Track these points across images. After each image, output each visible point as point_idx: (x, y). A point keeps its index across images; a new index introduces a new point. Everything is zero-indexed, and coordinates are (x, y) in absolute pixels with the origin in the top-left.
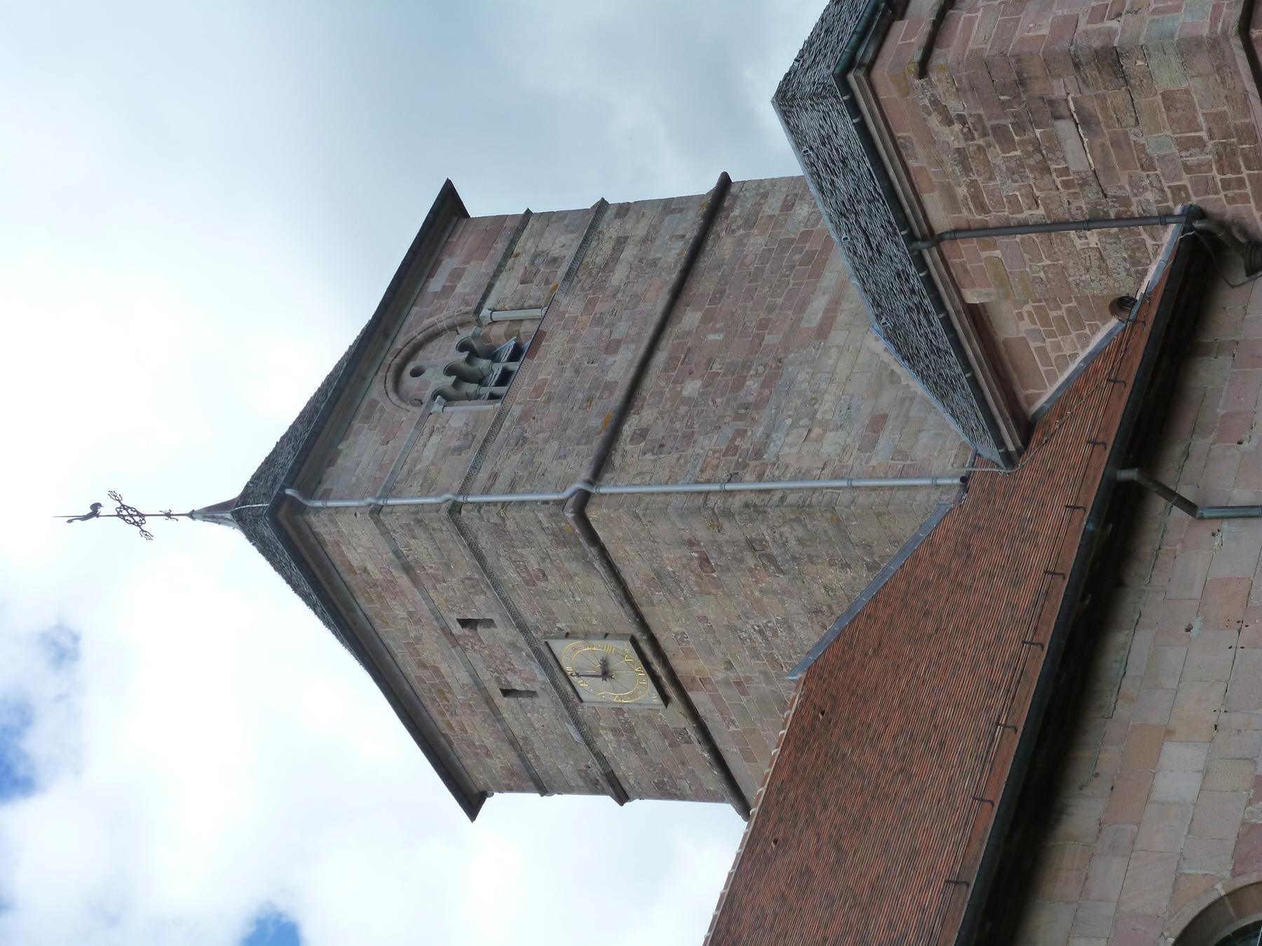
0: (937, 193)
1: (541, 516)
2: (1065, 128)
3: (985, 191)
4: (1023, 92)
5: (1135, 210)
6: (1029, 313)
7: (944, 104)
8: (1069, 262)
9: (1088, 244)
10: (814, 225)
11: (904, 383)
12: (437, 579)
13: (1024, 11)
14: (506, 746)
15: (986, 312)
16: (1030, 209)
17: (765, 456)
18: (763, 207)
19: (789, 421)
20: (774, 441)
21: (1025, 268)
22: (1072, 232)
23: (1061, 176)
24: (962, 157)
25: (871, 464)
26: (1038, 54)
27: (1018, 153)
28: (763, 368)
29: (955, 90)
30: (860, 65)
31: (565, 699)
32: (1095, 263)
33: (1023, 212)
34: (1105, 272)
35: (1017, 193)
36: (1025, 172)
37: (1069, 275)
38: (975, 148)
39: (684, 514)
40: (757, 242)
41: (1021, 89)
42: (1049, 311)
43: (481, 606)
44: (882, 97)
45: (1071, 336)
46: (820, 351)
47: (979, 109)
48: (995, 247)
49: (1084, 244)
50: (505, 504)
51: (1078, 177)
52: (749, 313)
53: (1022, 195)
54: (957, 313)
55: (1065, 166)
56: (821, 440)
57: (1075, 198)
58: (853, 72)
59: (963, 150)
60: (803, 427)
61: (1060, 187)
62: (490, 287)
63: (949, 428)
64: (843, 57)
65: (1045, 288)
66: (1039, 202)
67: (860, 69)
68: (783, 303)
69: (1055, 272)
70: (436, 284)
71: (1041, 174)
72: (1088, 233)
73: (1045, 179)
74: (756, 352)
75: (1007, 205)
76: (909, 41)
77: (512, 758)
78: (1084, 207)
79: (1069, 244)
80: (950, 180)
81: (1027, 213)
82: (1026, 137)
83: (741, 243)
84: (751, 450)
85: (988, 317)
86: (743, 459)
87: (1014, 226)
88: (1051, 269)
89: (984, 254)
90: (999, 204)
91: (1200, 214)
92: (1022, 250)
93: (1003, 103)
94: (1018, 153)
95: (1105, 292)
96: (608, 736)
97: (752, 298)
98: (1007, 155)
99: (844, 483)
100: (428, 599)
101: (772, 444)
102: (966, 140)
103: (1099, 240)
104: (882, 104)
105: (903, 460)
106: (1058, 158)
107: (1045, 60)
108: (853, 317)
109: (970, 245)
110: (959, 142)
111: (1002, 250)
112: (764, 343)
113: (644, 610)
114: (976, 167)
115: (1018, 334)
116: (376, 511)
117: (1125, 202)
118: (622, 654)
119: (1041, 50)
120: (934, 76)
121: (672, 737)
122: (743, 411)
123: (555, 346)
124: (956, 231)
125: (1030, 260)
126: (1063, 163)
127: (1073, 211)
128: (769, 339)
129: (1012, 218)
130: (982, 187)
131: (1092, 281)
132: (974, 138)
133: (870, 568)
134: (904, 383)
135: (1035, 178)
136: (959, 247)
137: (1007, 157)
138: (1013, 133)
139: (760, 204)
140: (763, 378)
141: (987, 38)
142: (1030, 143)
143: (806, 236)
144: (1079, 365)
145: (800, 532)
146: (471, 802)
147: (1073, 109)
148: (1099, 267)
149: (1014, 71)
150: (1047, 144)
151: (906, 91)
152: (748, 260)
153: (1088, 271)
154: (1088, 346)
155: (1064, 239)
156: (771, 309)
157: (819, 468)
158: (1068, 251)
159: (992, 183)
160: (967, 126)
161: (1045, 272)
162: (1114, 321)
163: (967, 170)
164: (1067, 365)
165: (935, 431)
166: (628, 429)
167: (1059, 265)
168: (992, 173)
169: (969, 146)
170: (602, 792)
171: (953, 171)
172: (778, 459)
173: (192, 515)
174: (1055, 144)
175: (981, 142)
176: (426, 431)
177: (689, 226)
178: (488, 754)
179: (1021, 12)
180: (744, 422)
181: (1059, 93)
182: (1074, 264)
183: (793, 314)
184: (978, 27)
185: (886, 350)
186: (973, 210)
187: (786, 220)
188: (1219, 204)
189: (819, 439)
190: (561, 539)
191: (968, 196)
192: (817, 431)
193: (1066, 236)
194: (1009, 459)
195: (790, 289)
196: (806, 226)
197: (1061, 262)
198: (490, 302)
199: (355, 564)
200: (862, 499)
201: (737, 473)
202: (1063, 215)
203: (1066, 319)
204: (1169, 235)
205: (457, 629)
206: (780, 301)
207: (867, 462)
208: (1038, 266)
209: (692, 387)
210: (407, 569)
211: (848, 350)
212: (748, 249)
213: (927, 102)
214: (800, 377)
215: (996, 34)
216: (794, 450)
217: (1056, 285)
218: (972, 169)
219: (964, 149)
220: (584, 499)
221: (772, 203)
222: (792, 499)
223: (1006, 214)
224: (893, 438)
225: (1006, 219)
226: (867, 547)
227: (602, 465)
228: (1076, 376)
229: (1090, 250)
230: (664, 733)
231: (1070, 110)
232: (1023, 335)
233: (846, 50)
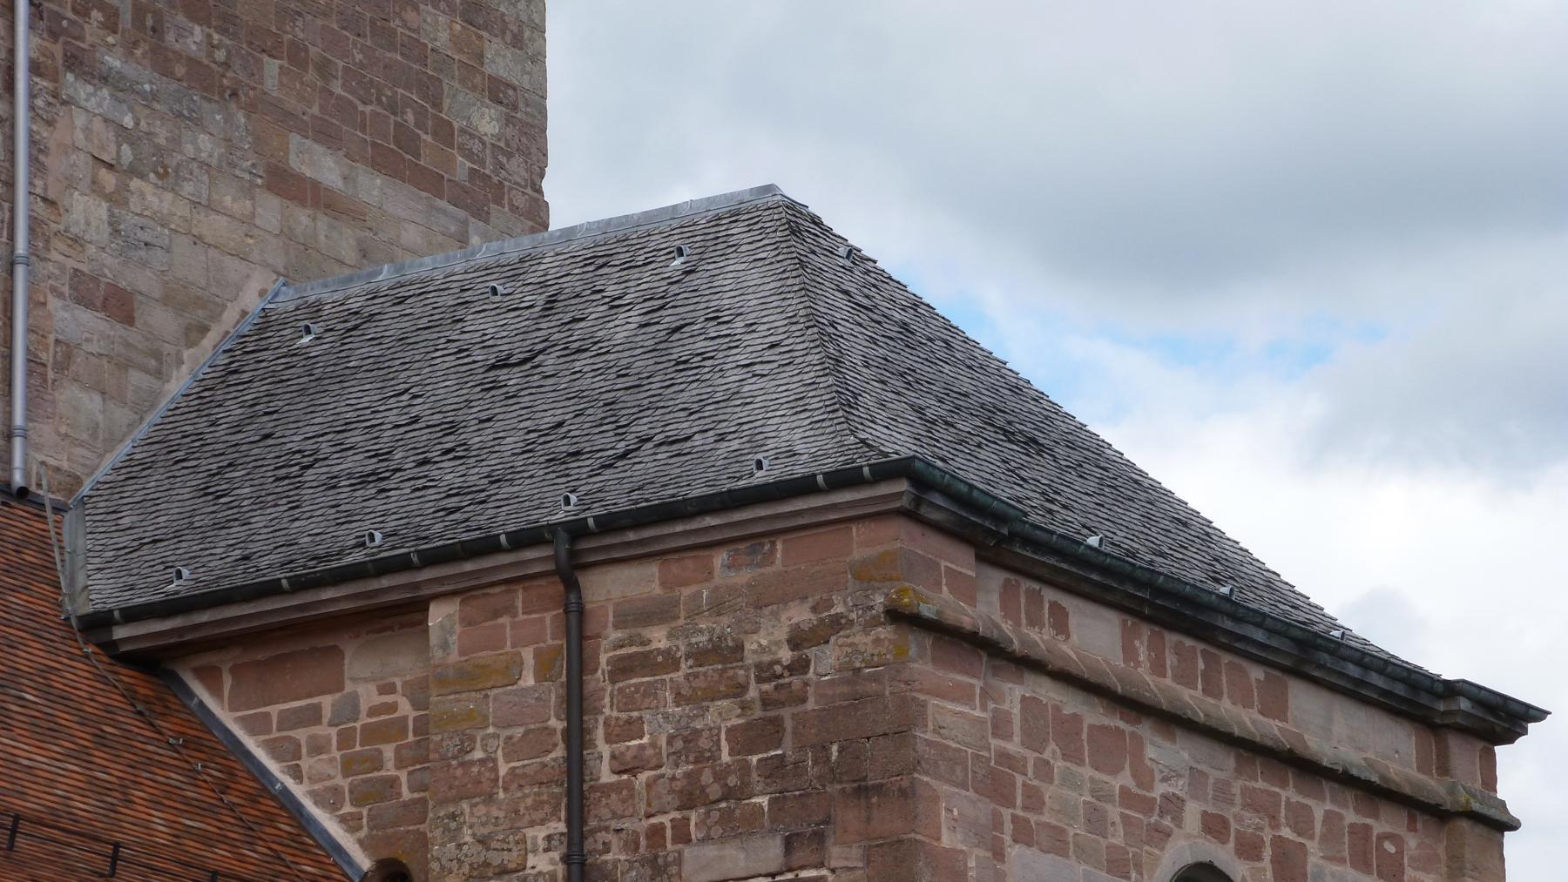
0: (657, 590)
3: (656, 681)
4: (843, 789)
6: (392, 707)
7: (833, 639)
8: (500, 809)
9: (535, 851)
10: (461, 148)
11: (186, 354)
13: (977, 796)
15: (402, 626)
16: (613, 757)
17: (70, 77)
18: (498, 40)
19: (128, 121)
20: (94, 95)
21: (494, 725)
22: (562, 827)
23: (673, 828)
24: (725, 652)
25: (50, 298)
26: (913, 831)
27: (725, 757)
28: (223, 59)
29: (858, 665)
30: (918, 501)
32: (496, 859)
33: (607, 742)
34: (475, 873)
35: (645, 740)
36: (687, 763)
37: (473, 806)
38: (741, 680)
41: (848, 786)
42: (394, 745)
44: (854, 530)
45: (340, 776)
46: (247, 177)
47: (816, 702)
48: (542, 674)
49: (535, 844)
51: (670, 859)
52: (319, 22)
53: (642, 747)
54: (416, 586)
55: (693, 837)
56: (93, 191)
57: (626, 843)
58: (911, 490)
59: (739, 656)
60: (118, 152)
61: (653, 820)
63: (106, 452)
64: (937, 472)
65: (450, 755)
66: (625, 777)
67: (913, 500)
68: (332, 93)
69: (484, 780)
71: (681, 792)
72: (556, 855)
73: (670, 798)
74: (250, 44)
75: (624, 716)
76: (944, 582)
78: (609, 857)
79: (538, 815)
80: (681, 621)
81: (605, 749)
82: (755, 776)
84: (82, 45)
85: (391, 628)
86: (66, 29)
87: (582, 720)
88: (487, 774)
89: (528, 655)
90: (627, 702)
92: (532, 727)
93: (825, 749)
94: (725, 757)
95: (435, 866)
97: (344, 28)
98: (723, 736)
99: (21, 247)
101: (90, 89)
102: (758, 666)
103: (540, 873)
104: (843, 526)
105: (55, 363)
106: (710, 828)
107: (900, 842)
108: (302, 241)
109: (549, 631)
110: (755, 652)
111: (533, 689)
112: (266, 58)
114: (705, 674)
115: (351, 679)
119: (919, 837)
120: (885, 632)
122: (149, 22)
124: (581, 612)
125: (510, 738)
126: (700, 836)
127: (602, 836)
128: (272, 67)
129: (597, 720)
130: (664, 677)
131: (459, 846)
132: (760, 680)
134: (186, 354)
135: (673, 778)
136: (547, 610)
137: (718, 735)
138: (765, 755)
139: (504, 33)
140: (206, 62)
141: (942, 731)
142: (742, 783)
143: (444, 132)
144: (277, 780)
147: (804, 874)
148: (486, 864)
149: (883, 781)
150: (738, 812)
151: (866, 575)
152: (410, 15)
153: (479, 841)
154: (316, 803)
155: (547, 809)
156: (324, 69)
157: (45, 189)
158: (522, 811)
159: (669, 696)
160: (786, 673)
161: (482, 762)
162: (365, 863)
163: (699, 656)
164: (278, 757)
165: (101, 425)
167: (495, 790)
168: (688, 700)
169: (747, 669)
171: (701, 631)
172: (64, 103)
174: (737, 827)
175: (752, 693)
179: (976, 792)
180: (129, 26)
182: (497, 818)
183: (313, 116)
184: (960, 712)
185: (244, 313)
186: (618, 652)
187: (474, 88)
189: (96, 187)
191: (647, 648)
192: (109, 179)
193: (556, 809)
194: (96, 624)
195: (355, 107)
196: (463, 131)
197: (501, 795)
201: (41, 18)
202: (596, 816)
203: (376, 774)
206: (337, 88)
207: (54, 290)
208: (496, 752)
211: (247, 235)
212: (428, 12)
213: (839, 609)
214: (204, 141)
215: (947, 747)
216: (79, 136)
217: (455, 778)
218: (701, 666)
219: (742, 659)
221: (504, 56)
223: (607, 711)
224: (92, 340)
225: (595, 708)
228: (253, 770)
229: (523, 852)
231: (803, 868)
232: (349, 687)
233: (947, 476)
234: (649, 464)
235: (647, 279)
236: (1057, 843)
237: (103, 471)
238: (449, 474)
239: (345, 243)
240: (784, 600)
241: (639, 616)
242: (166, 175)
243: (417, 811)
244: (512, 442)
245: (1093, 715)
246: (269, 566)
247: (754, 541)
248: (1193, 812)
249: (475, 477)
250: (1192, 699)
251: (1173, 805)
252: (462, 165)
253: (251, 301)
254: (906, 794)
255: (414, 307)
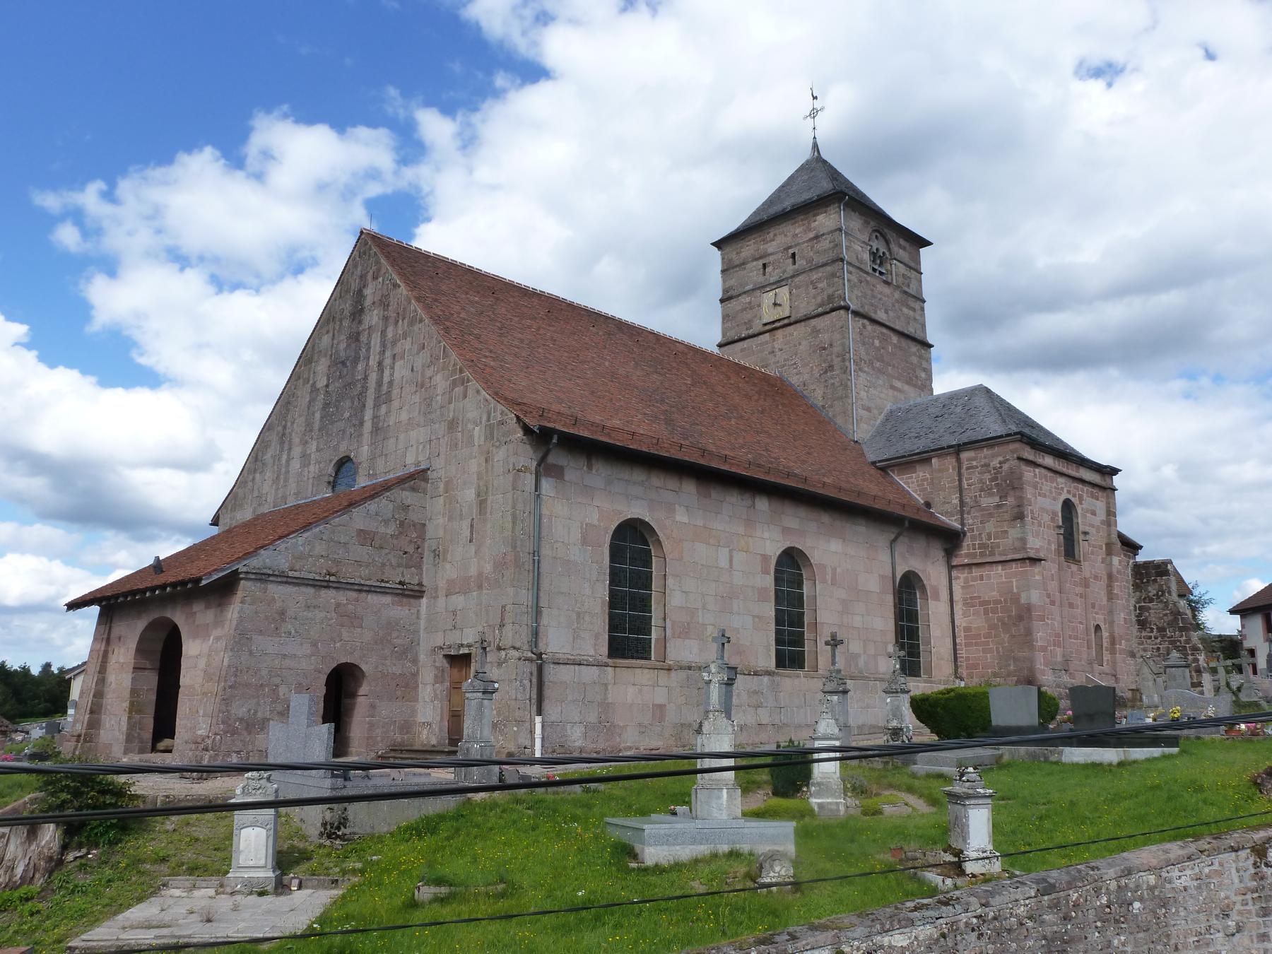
1: (839, 292)
2: (997, 499)
5: (965, 516)
12: (812, 247)
14: (741, 261)
24: (987, 465)
31: (764, 287)
39: (843, 345)
40: (915, 360)
43: (801, 263)
48: (953, 469)
50: (844, 279)
62: (901, 262)
70: (902, 242)
77: (737, 262)
83: (915, 354)
91: (965, 534)
96: (748, 300)
100: (804, 242)
113: (803, 323)
116: (840, 230)
117: (969, 513)
118: (784, 311)
121: (749, 324)
123: (887, 290)
133: (823, 406)
143: (917, 377)
145: (837, 384)
146: (719, 244)
151: (1012, 452)
163: (982, 466)
166: (865, 321)
170: (724, 293)
173: (815, 138)
174: (991, 495)
176: (862, 245)
177: (918, 335)
178: (737, 253)
181: (1009, 499)
188: (967, 542)
189: (864, 390)
190: (831, 298)
194: (874, 463)
198: (898, 263)
199: (818, 218)
200: (850, 407)
204: (957, 525)
205: (791, 251)
209: (877, 343)
210: (817, 237)
220: (847, 308)
222: (849, 383)
226: (831, 406)
227: (856, 313)
230: (750, 321)
234: (969, 433)
235: (961, 401)
236: (1045, 496)
237: (868, 437)
238: (931, 436)
239: (901, 396)
240: (997, 456)
241: (970, 459)
242: (875, 388)
243: (931, 493)
244: (942, 430)
245: (1049, 474)
246: (901, 453)
247: (992, 446)
248: (1065, 491)
249: (937, 436)
250: (1065, 470)
251: (1062, 488)
252: (920, 383)
253: (888, 407)
254: (1022, 489)
255: (918, 407)
